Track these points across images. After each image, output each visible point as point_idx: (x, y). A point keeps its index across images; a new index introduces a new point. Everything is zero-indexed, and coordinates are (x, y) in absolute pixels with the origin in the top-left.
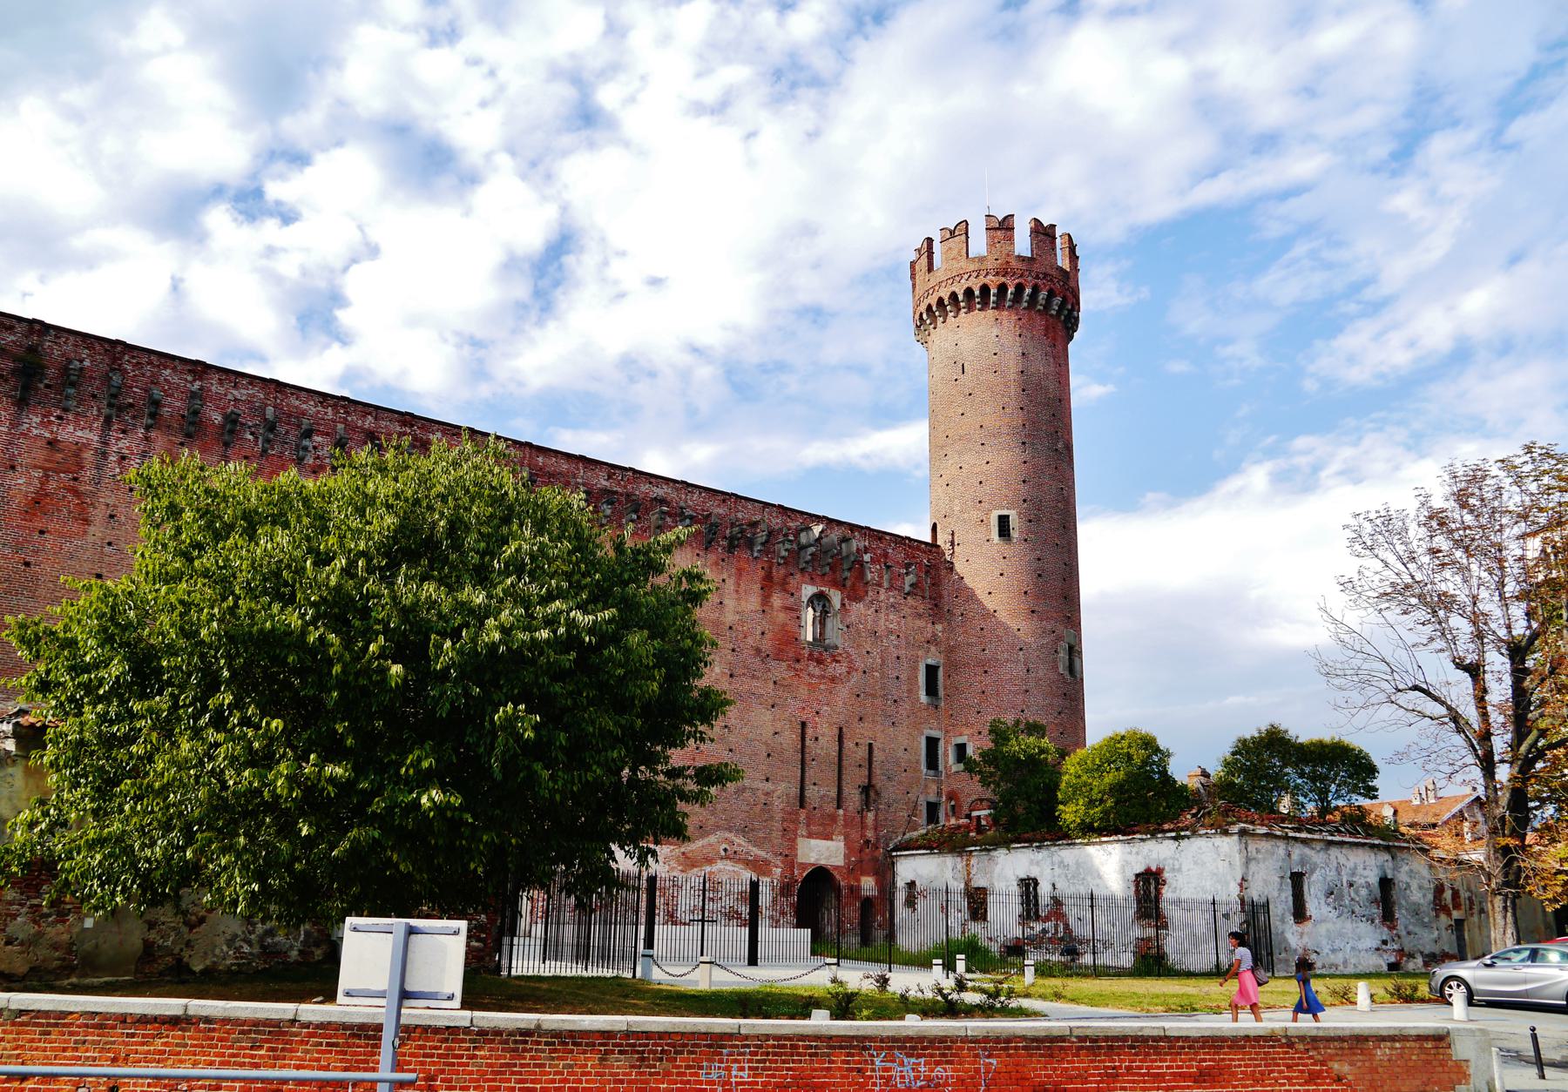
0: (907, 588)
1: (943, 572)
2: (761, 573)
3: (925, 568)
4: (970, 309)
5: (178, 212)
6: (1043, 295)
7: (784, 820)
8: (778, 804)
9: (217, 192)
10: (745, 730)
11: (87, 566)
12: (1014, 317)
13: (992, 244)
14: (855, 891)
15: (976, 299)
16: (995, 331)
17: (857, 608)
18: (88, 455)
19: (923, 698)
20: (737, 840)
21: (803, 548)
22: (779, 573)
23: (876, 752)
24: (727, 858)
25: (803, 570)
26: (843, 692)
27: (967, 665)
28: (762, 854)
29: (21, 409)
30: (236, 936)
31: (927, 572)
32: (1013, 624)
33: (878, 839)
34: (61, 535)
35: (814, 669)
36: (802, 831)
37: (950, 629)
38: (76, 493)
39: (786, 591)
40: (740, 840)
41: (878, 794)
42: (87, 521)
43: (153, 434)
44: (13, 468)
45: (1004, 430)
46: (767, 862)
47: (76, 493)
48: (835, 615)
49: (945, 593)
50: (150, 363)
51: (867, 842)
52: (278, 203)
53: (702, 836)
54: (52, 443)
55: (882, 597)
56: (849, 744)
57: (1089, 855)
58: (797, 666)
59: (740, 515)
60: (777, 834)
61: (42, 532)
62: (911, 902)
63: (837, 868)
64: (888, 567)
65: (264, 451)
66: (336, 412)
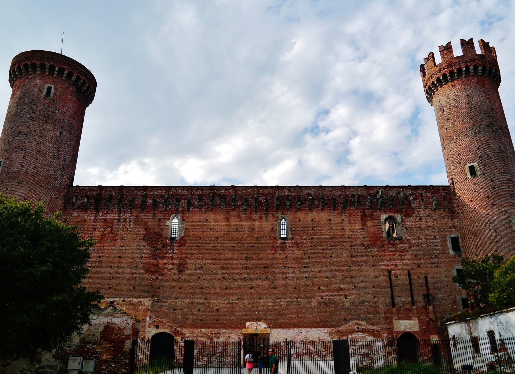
0: (434, 207)
1: (453, 196)
2: (360, 214)
3: (442, 198)
4: (441, 86)
5: (296, 140)
6: (472, 68)
7: (385, 313)
8: (381, 307)
9: (306, 131)
10: (361, 278)
11: (116, 255)
12: (460, 82)
13: (443, 57)
14: (428, 342)
15: (440, 82)
16: (453, 91)
17: (409, 220)
18: (115, 221)
19: (451, 252)
20: (363, 324)
21: (378, 200)
22: (368, 212)
23: (429, 279)
24: (359, 331)
25: (380, 209)
26: (407, 257)
27: (468, 234)
28: (377, 328)
29: (97, 212)
30: (24, 369)
31: (444, 198)
32: (484, 213)
33: (436, 317)
34: (109, 246)
35: (391, 248)
36: (395, 317)
37: (459, 220)
38: (112, 233)
39: (373, 219)
40: (364, 323)
41: (434, 298)
42: (116, 241)
43: (133, 211)
44: (95, 229)
45: (465, 130)
46: (379, 332)
47: (112, 233)
48: (399, 224)
49: (455, 205)
50: (131, 190)
51: (431, 319)
52: (323, 128)
53: (346, 323)
54: (105, 220)
55: (422, 213)
56: (414, 278)
57: (509, 317)
58: (383, 248)
59: (347, 193)
60: (382, 320)
61: (104, 247)
62: (455, 346)
63: (415, 332)
64: (423, 200)
65: (166, 209)
66: (188, 192)
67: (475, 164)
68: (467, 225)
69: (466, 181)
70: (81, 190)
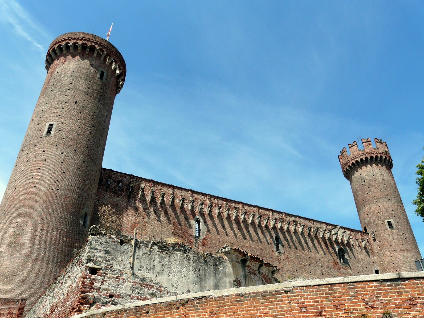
67: (391, 220)
68: (388, 262)
69: (386, 231)
70: (113, 174)
